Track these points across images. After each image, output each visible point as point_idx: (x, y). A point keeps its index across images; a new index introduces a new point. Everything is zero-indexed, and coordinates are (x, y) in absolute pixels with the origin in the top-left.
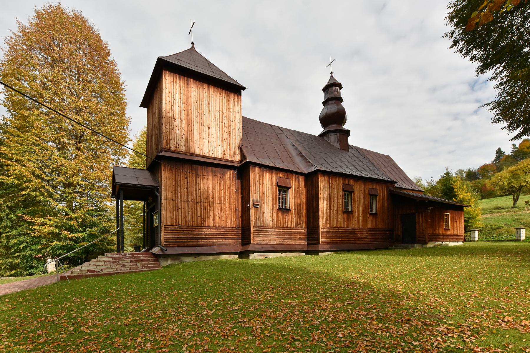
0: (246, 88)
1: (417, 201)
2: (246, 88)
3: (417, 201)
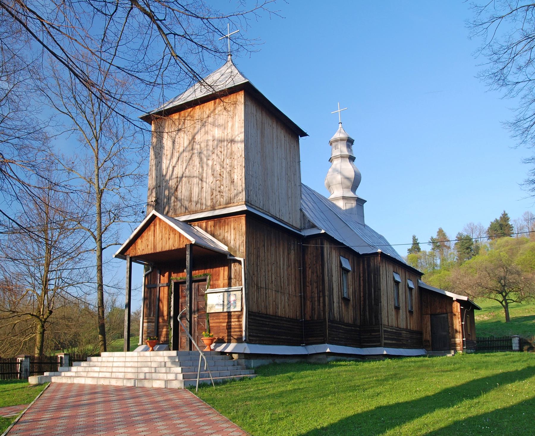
0: (307, 135)
2: (307, 135)
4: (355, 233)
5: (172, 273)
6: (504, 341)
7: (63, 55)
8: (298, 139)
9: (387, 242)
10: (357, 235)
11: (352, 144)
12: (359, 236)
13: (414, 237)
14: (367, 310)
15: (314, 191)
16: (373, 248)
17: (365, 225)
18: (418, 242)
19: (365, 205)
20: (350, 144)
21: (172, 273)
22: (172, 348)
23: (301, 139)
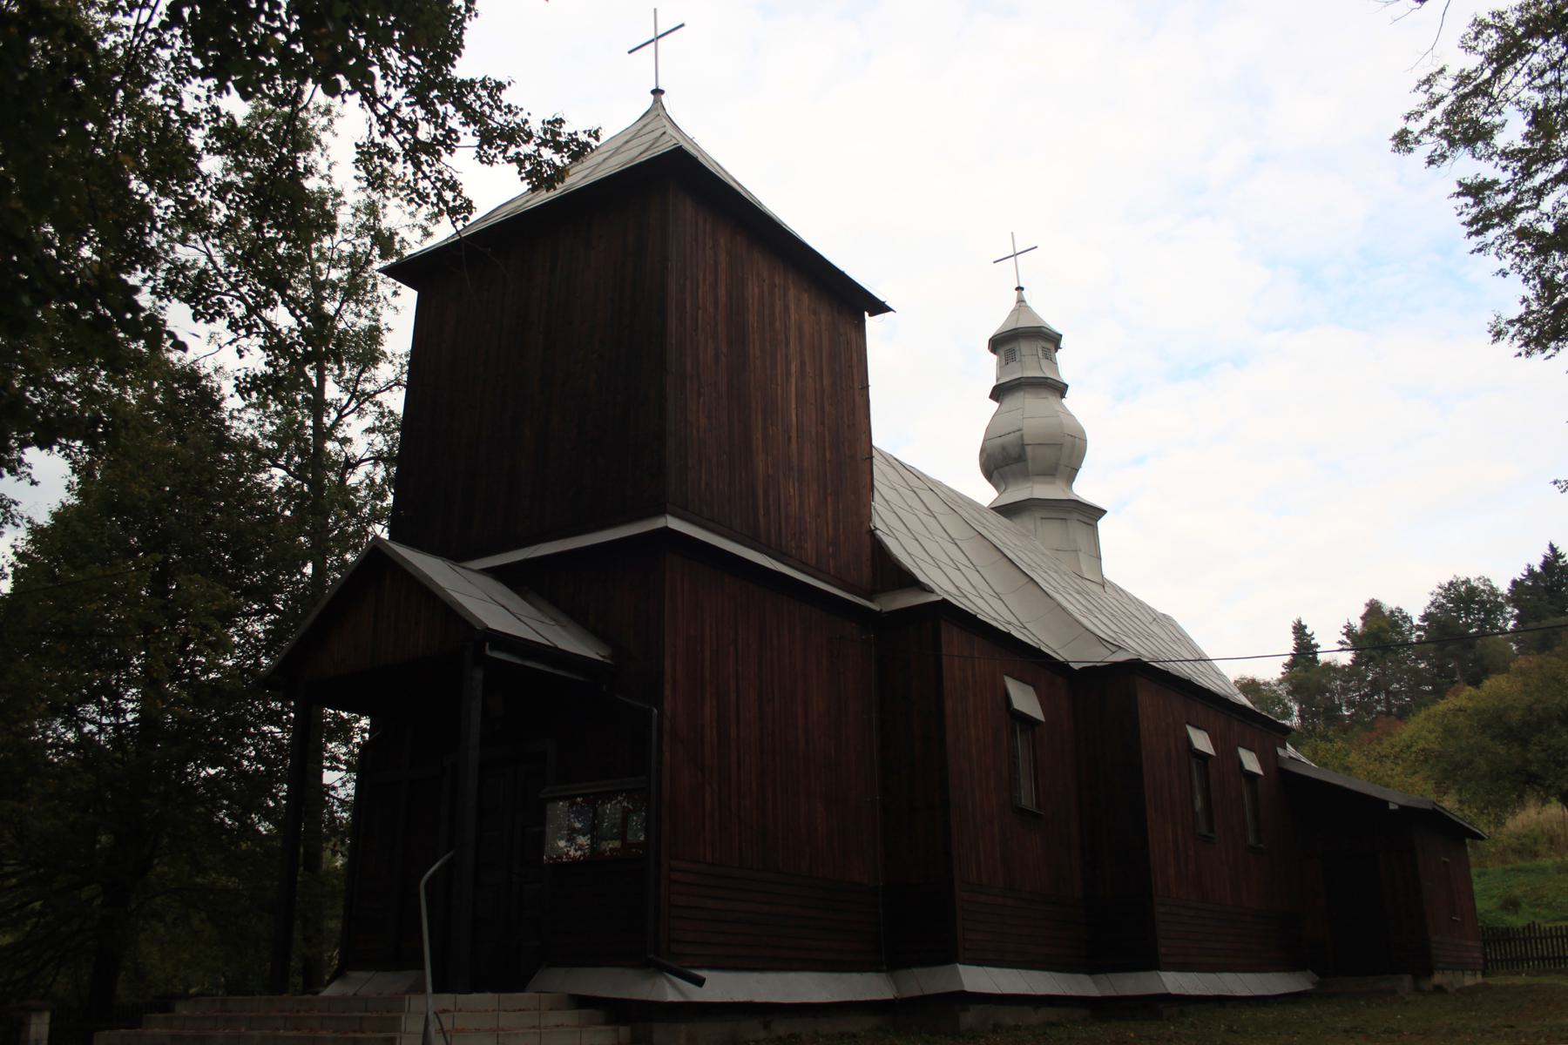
0: (888, 309)
1: (1392, 807)
2: (888, 309)
3: (1392, 807)
4: (1059, 605)
5: (866, 314)
6: (1554, 959)
7: (1105, 643)
8: (863, 321)
9: (1194, 648)
10: (1064, 609)
11: (1057, 347)
12: (1070, 615)
13: (1299, 630)
14: (528, 664)
15: (938, 484)
16: (1114, 649)
17: (1103, 583)
18: (1313, 642)
19: (1101, 523)
20: (1051, 346)
21: (866, 314)
22: (429, 988)
23: (872, 323)
